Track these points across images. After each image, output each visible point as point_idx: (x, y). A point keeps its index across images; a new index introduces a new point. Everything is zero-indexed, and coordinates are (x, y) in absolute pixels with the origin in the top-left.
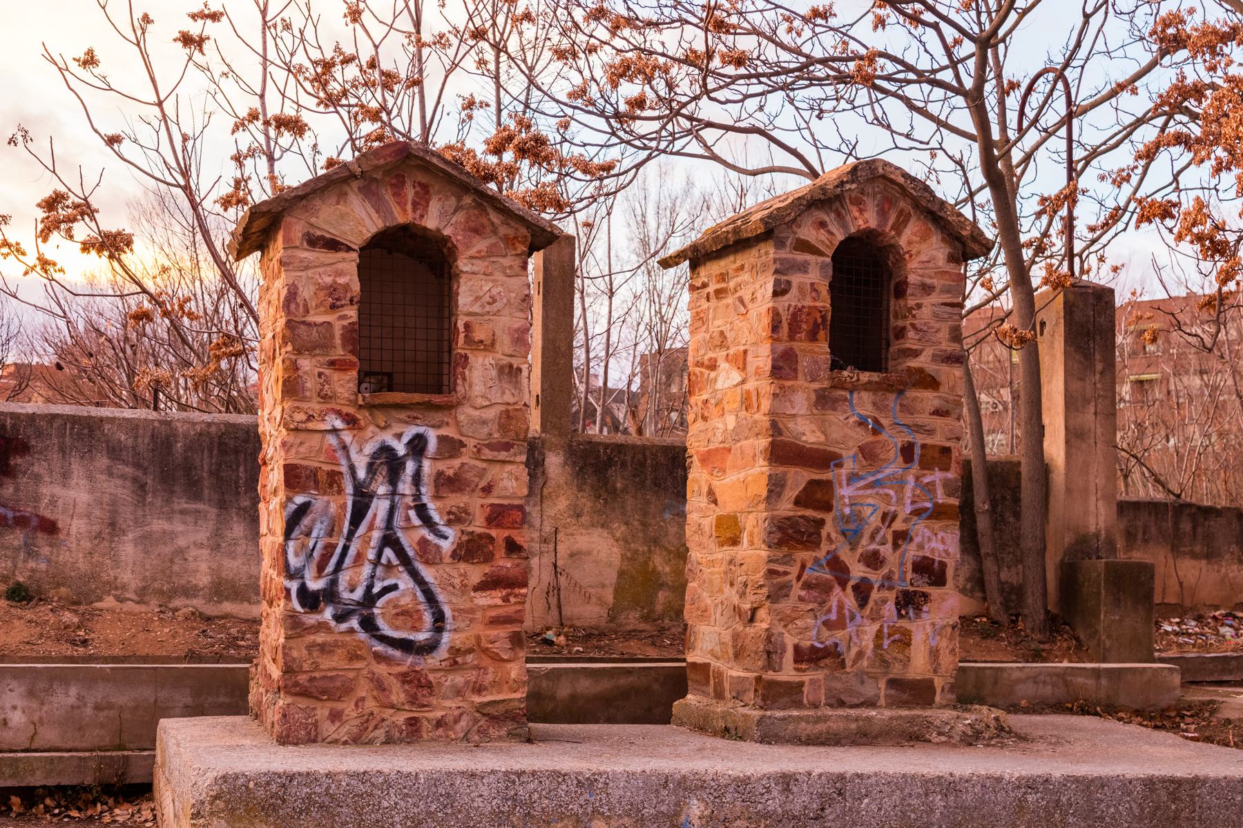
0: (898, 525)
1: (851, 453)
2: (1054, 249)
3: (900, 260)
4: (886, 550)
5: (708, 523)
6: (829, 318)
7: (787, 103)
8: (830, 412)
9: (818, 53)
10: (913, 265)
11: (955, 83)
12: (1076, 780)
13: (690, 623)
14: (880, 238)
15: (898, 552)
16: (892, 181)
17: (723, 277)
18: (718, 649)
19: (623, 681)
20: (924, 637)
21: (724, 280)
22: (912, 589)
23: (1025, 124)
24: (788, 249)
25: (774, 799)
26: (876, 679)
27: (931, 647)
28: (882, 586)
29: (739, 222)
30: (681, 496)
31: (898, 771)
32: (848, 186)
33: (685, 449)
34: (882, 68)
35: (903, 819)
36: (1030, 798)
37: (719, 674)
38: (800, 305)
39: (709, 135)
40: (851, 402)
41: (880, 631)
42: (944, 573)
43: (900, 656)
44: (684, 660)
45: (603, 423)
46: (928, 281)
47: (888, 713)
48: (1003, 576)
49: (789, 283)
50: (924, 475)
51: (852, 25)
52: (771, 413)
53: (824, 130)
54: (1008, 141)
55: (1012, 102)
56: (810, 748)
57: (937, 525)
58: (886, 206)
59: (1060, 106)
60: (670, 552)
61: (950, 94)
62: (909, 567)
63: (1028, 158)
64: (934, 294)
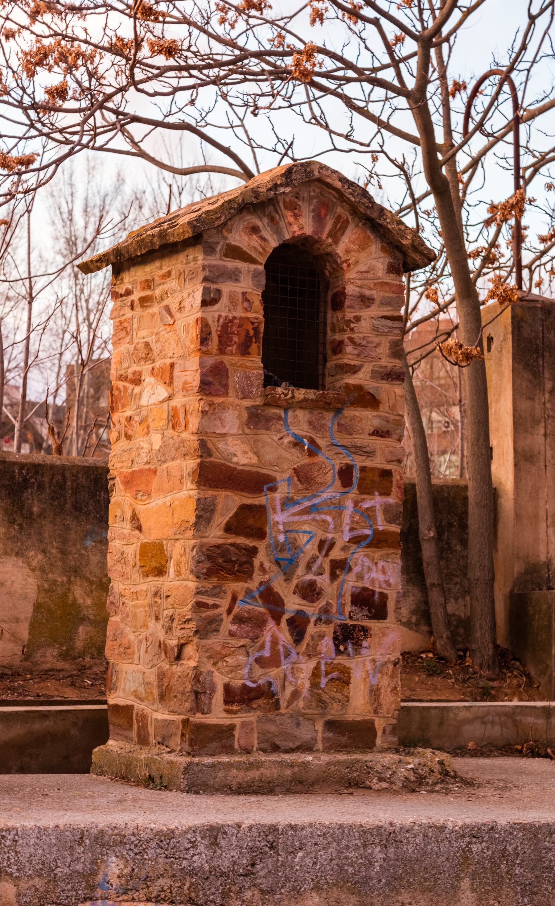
0: (336, 554)
1: (286, 476)
2: (502, 260)
3: (338, 269)
4: (323, 581)
5: (132, 552)
6: (262, 330)
7: (219, 98)
8: (263, 431)
9: (253, 46)
10: (351, 275)
11: (396, 83)
12: (523, 827)
13: (111, 661)
14: (316, 246)
15: (336, 583)
16: (329, 185)
17: (148, 284)
18: (141, 689)
19: (37, 726)
20: (364, 675)
21: (149, 287)
22: (351, 623)
23: (471, 127)
24: (218, 256)
25: (200, 854)
26: (312, 720)
27: (372, 686)
28: (319, 620)
29: (166, 226)
30: (103, 521)
31: (334, 821)
32: (282, 190)
33: (108, 471)
34: (321, 64)
35: (339, 873)
36: (475, 848)
37: (143, 718)
38: (230, 316)
39: (135, 129)
40: (285, 420)
41: (317, 668)
42: (385, 605)
43: (339, 696)
44: (105, 702)
45: (23, 439)
46: (367, 293)
47: (325, 758)
48: (451, 608)
49: (219, 292)
50: (363, 500)
51: (291, 18)
52: (200, 432)
53: (258, 127)
54: (452, 146)
55: (458, 104)
56: (241, 797)
57: (377, 553)
58: (323, 212)
59: (506, 109)
60: (91, 583)
61: (391, 94)
62: (348, 599)
63: (475, 163)
64: (373, 307)
